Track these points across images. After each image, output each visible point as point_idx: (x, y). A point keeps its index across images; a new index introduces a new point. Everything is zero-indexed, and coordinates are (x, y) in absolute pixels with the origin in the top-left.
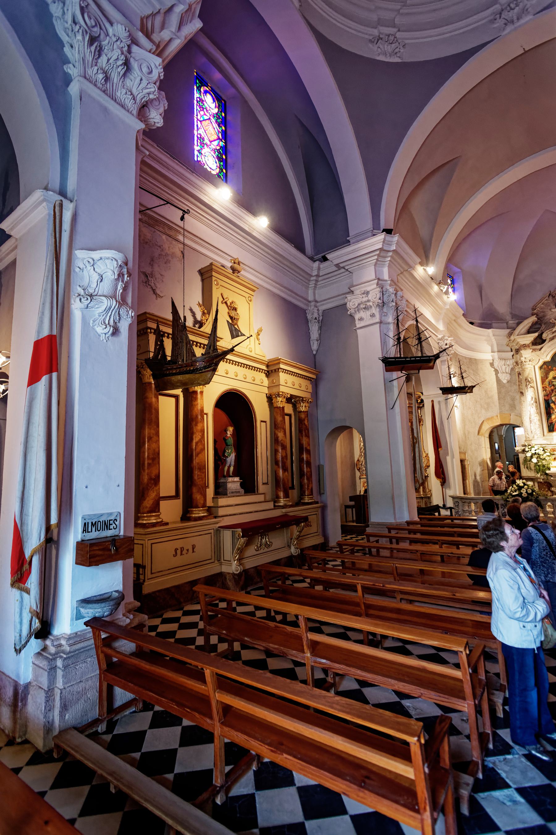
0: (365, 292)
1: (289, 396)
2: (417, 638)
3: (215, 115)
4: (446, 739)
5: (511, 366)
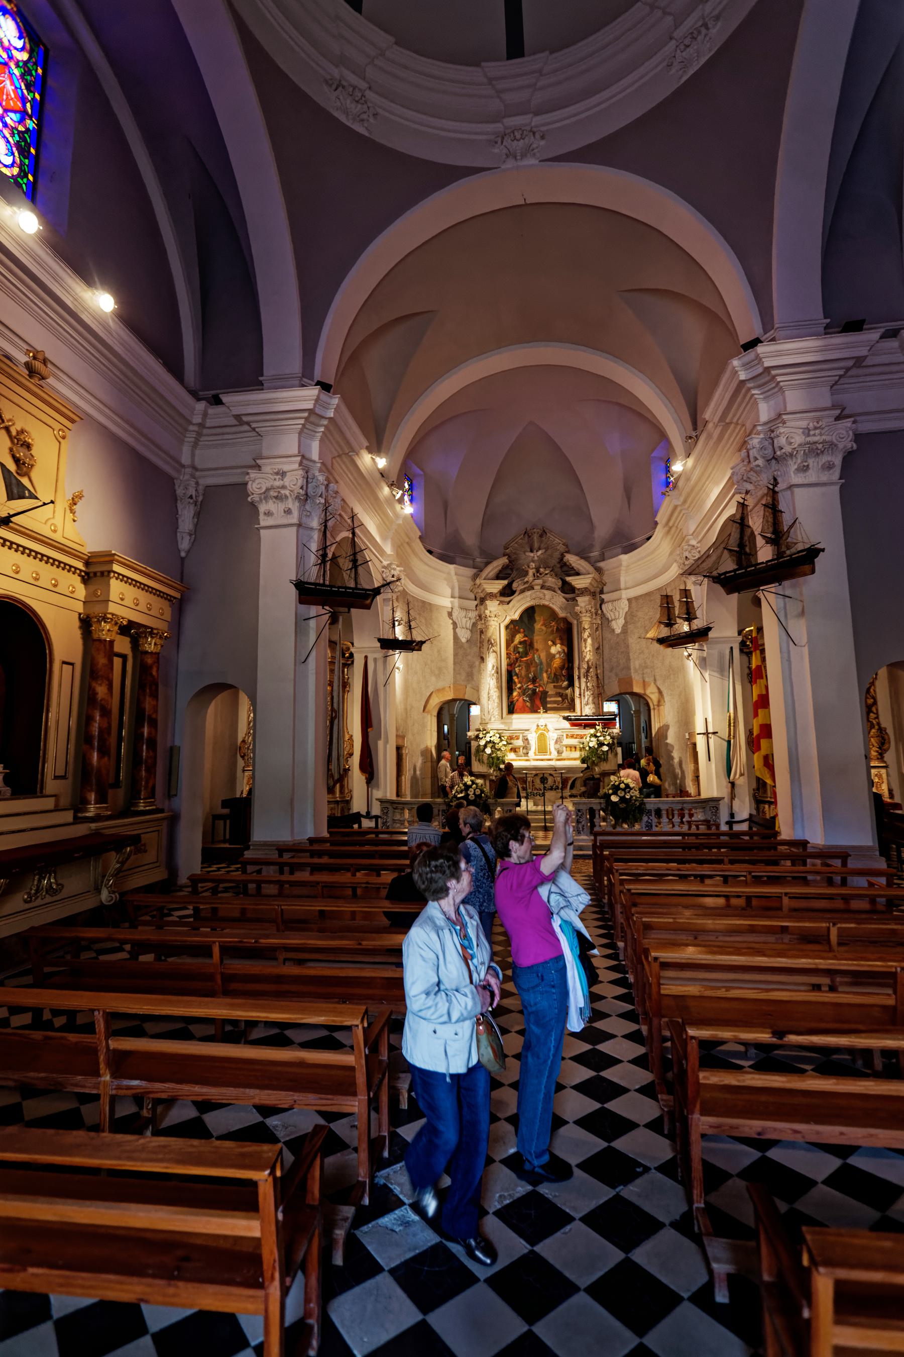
0: (279, 470)
1: (125, 623)
2: (295, 1016)
3: (21, 64)
4: (318, 1162)
5: (473, 621)
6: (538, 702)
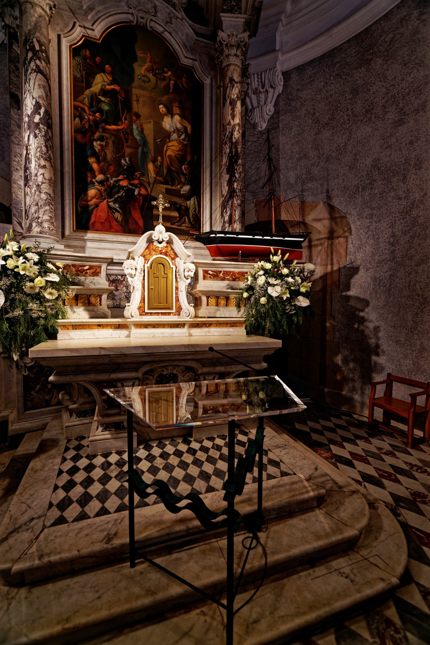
6: (137, 215)
